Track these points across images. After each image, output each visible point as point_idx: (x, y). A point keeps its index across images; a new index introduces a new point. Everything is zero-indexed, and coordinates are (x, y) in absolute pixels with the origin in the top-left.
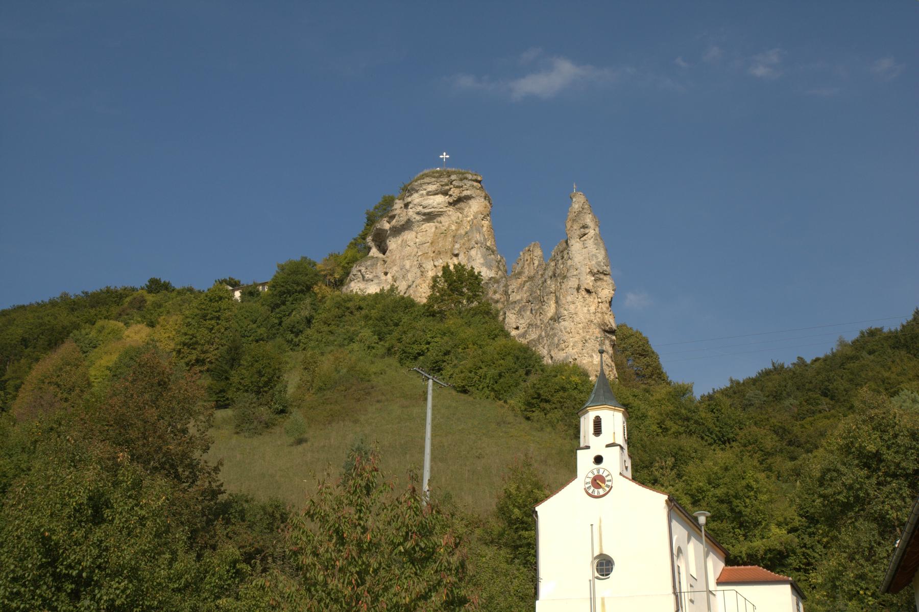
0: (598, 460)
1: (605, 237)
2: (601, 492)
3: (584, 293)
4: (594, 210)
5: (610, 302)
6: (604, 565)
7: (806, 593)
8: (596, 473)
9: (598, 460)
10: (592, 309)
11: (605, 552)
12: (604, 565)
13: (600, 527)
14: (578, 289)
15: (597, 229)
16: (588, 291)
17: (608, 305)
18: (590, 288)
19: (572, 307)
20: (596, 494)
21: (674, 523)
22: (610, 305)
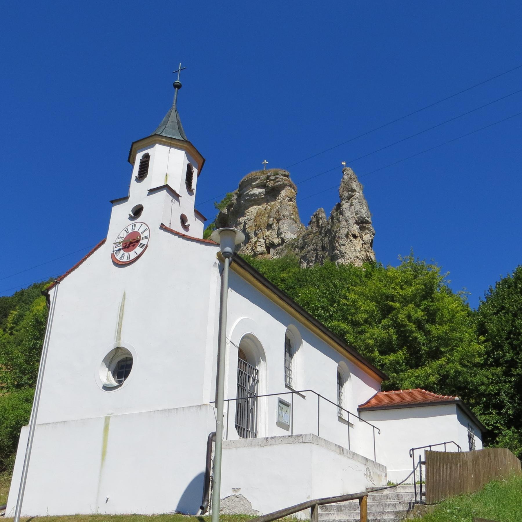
0: (138, 211)
1: (369, 196)
2: (132, 255)
3: (351, 238)
4: (361, 179)
5: (371, 243)
6: (121, 366)
7: (486, 343)
8: (130, 230)
9: (138, 211)
10: (358, 248)
11: (125, 343)
12: (121, 366)
13: (122, 307)
14: (347, 236)
15: (361, 192)
16: (355, 237)
17: (369, 245)
18: (357, 233)
19: (343, 248)
20: (125, 260)
21: (232, 295)
22: (371, 246)
